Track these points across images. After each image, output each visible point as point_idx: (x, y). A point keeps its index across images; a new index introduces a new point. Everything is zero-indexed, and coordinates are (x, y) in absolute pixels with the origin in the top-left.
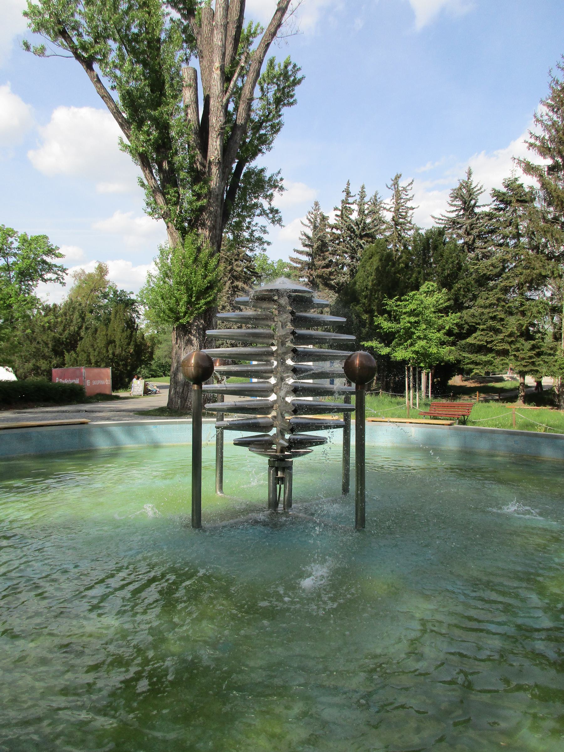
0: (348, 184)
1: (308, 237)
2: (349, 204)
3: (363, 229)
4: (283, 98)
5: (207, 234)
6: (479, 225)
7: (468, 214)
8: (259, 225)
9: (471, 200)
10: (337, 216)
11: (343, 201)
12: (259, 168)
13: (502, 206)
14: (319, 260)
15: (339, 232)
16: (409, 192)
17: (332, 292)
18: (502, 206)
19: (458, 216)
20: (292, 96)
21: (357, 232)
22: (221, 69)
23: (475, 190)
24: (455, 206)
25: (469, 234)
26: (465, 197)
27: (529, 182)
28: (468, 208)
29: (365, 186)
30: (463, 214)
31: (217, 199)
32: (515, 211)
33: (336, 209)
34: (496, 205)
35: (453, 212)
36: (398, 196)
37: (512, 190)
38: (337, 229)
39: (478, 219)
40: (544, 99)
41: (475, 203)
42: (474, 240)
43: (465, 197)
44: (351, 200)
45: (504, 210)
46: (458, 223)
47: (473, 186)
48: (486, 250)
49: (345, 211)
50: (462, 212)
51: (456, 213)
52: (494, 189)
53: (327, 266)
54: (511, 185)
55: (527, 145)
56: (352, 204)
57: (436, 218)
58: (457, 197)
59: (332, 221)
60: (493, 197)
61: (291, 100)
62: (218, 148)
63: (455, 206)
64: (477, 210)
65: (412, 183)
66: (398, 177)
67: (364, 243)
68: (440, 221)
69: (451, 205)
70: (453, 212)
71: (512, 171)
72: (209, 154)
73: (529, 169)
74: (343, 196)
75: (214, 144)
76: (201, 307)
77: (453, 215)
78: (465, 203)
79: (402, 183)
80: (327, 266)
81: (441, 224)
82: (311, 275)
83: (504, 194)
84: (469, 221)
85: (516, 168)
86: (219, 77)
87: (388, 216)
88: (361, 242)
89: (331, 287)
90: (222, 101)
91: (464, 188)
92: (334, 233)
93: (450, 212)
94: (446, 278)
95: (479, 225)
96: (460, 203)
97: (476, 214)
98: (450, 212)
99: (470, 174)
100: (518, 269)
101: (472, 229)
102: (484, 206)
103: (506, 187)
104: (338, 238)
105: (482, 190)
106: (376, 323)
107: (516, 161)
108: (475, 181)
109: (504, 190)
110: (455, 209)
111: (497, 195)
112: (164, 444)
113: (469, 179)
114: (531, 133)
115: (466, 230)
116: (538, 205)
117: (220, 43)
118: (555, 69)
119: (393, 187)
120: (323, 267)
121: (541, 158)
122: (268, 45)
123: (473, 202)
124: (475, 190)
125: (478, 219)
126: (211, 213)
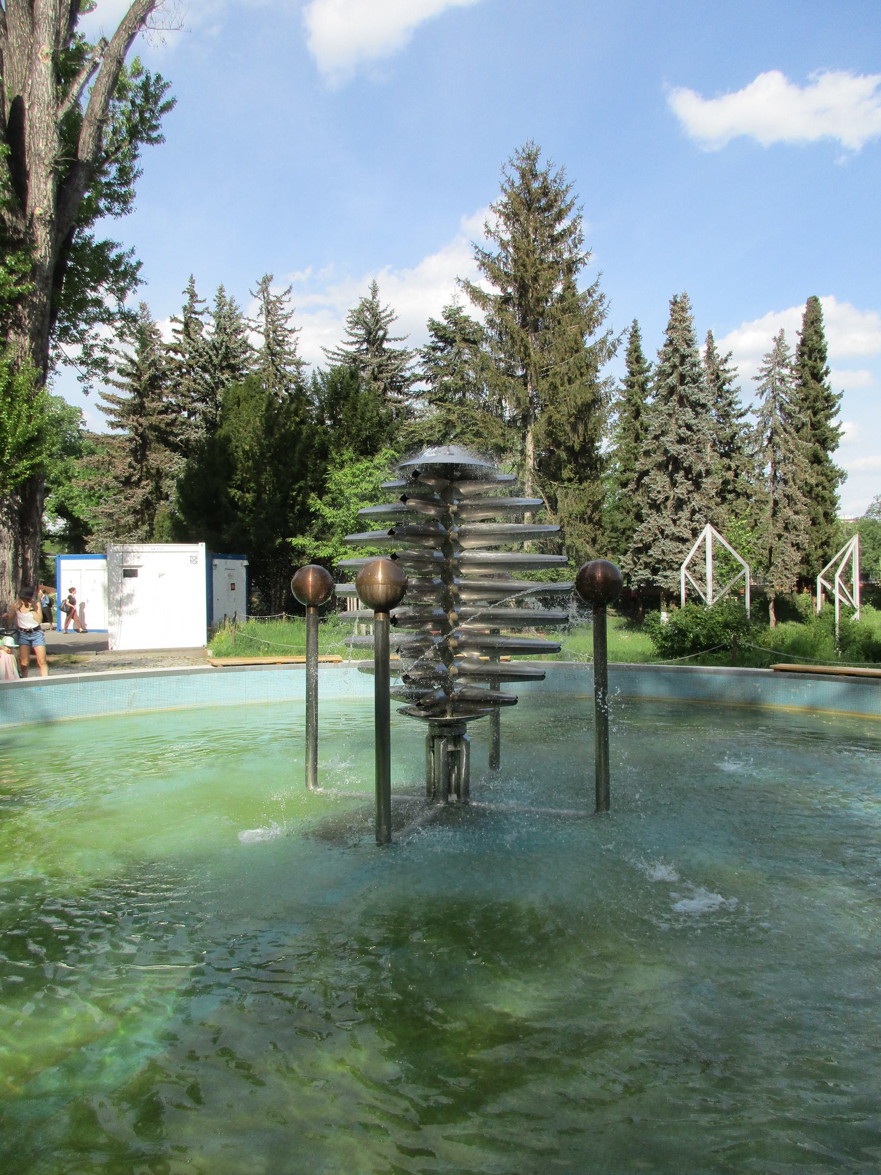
0: (192, 281)
1: (132, 361)
2: (195, 313)
3: (226, 357)
4: (141, 129)
5: (27, 343)
6: (390, 367)
7: (374, 349)
8: (102, 337)
9: (379, 329)
10: (175, 331)
11: (185, 308)
12: (97, 241)
13: (441, 344)
14: (153, 400)
15: (179, 357)
16: (284, 305)
17: (177, 456)
18: (441, 344)
19: (359, 350)
20: (155, 128)
21: (216, 361)
22: (53, 59)
23: (383, 315)
24: (356, 335)
25: (376, 379)
26: (371, 326)
27: (477, 315)
28: (375, 341)
29: (225, 288)
30: (367, 349)
31: (46, 286)
32: (459, 353)
33: (174, 320)
34: (433, 342)
35: (352, 343)
36: (270, 309)
37: (456, 324)
38: (176, 352)
39: (389, 358)
40: (494, 204)
41: (385, 335)
42: (385, 390)
43: (371, 326)
44: (198, 307)
45: (442, 350)
46: (362, 362)
47: (380, 309)
48: (403, 405)
49: (189, 327)
50: (365, 346)
51: (357, 346)
52: (431, 320)
53: (165, 411)
54: (453, 315)
55: (478, 263)
56: (201, 313)
57: (329, 352)
58: (357, 323)
59: (168, 338)
60: (430, 330)
61: (154, 135)
62: (50, 195)
63: (356, 335)
64: (386, 345)
65: (289, 291)
66: (267, 280)
67: (227, 379)
68: (336, 356)
69: (351, 334)
70: (352, 343)
71: (454, 297)
72: (31, 202)
73: (477, 296)
74: (186, 300)
75: (42, 186)
76: (22, 473)
77: (352, 349)
78: (369, 333)
79: (275, 290)
80: (165, 411)
81: (335, 360)
82: (141, 425)
83: (445, 328)
84: (376, 361)
85: (461, 294)
86: (50, 72)
87: (257, 341)
88: (223, 378)
89: (174, 448)
90: (55, 114)
91: (368, 310)
92: (172, 359)
93: (347, 343)
94: (364, 442)
95: (390, 367)
96: (362, 332)
97: (384, 351)
98: (347, 343)
99: (375, 291)
100: (467, 436)
101: (381, 372)
102: (396, 340)
103: (446, 318)
104: (179, 368)
105: (394, 317)
106: (312, 510)
107: (462, 284)
108: (384, 302)
109: (444, 322)
110: (355, 340)
111: (435, 328)
112: (58, 719)
113: (374, 297)
114: (476, 247)
115: (373, 373)
116: (485, 347)
117: (51, 13)
118: (508, 166)
119: (261, 295)
120: (161, 413)
121: (489, 284)
122: (131, 37)
123: (381, 333)
124: (383, 315)
125: (389, 358)
126: (33, 306)
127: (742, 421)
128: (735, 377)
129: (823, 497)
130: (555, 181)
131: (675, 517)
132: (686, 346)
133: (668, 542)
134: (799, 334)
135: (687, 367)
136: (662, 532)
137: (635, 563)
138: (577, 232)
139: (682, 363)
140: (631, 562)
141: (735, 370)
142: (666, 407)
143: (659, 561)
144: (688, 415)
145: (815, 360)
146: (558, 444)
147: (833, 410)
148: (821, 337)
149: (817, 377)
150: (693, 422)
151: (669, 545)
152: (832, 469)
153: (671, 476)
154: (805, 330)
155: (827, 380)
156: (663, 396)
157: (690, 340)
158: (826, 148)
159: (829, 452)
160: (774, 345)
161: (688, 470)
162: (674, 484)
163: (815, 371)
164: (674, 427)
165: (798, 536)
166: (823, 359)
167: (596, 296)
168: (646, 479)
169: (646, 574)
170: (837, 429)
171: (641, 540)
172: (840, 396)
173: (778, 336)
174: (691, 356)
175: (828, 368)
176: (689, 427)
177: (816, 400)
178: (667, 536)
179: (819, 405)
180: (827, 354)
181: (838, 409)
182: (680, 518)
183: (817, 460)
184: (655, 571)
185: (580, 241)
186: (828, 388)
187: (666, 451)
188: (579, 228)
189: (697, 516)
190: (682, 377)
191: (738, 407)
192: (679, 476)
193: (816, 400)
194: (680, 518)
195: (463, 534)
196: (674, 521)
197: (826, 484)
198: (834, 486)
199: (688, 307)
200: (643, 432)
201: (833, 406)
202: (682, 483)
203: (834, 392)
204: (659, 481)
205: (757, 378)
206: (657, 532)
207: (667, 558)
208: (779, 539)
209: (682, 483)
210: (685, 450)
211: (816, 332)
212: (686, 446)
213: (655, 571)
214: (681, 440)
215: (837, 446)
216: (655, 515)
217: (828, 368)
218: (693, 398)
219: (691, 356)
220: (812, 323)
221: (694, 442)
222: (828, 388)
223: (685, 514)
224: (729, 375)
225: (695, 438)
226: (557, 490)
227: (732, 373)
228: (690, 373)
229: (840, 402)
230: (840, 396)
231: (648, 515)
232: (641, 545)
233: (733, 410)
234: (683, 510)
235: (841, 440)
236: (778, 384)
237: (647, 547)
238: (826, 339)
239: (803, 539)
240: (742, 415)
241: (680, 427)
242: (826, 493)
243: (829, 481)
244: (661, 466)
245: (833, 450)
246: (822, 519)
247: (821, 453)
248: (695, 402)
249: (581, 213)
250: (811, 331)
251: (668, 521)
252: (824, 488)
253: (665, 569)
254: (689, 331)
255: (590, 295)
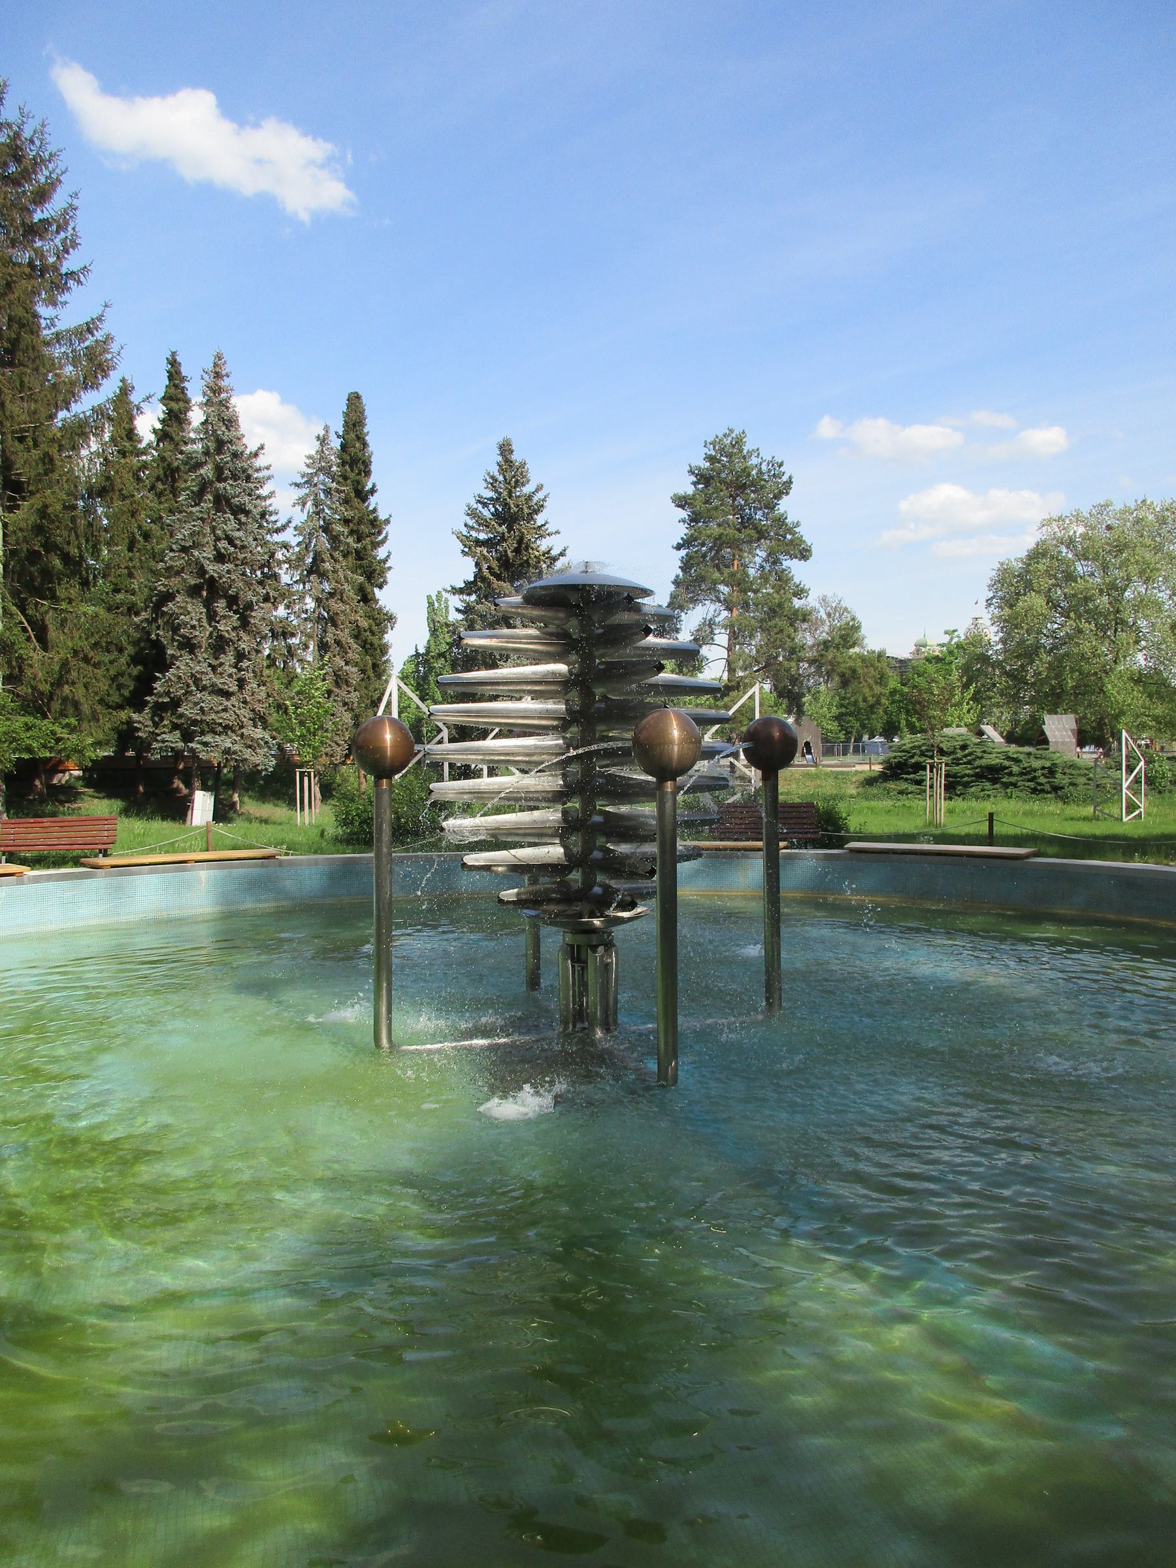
127: (277, 538)
128: (269, 478)
129: (372, 644)
130: (32, 142)
131: (215, 663)
132: (224, 428)
133: (206, 696)
134: (339, 437)
135: (226, 457)
136: (197, 681)
137: (156, 725)
138: (70, 228)
139: (219, 451)
140: (150, 723)
141: (268, 468)
142: (198, 508)
143: (195, 722)
144: (229, 525)
145: (359, 474)
146: (50, 547)
147: (380, 538)
148: (365, 445)
149: (362, 495)
150: (237, 534)
151: (210, 700)
152: (380, 610)
153: (208, 604)
154: (346, 432)
155: (373, 501)
156: (192, 492)
157: (229, 421)
158: (265, 208)
159: (376, 590)
160: (317, 445)
161: (232, 601)
162: (212, 616)
163: (360, 487)
164: (210, 539)
165: (349, 692)
166: (368, 473)
167: (99, 335)
168: (170, 607)
169: (173, 739)
170: (385, 561)
171: (168, 693)
172: (387, 521)
173: (322, 433)
174: (231, 442)
175: (374, 486)
176: (231, 541)
177: (360, 522)
178: (204, 688)
179: (364, 529)
180: (373, 468)
181: (386, 537)
182: (221, 664)
183: (366, 598)
184: (187, 737)
185: (74, 245)
186: (375, 510)
187: (202, 571)
188: (72, 224)
189: (245, 664)
190: (219, 470)
191: (273, 518)
192: (220, 605)
193: (360, 522)
194: (221, 664)
195: (558, 797)
196: (214, 668)
197: (375, 628)
198: (384, 632)
199: (224, 373)
200: (141, 539)
201: (380, 533)
202: (224, 617)
203: (382, 516)
204: (191, 612)
205: (297, 485)
206: (190, 682)
207: (208, 718)
208: (329, 697)
209: (224, 617)
210: (229, 572)
211: (358, 438)
212: (231, 566)
213: (187, 737)
214: (220, 558)
215: (385, 582)
216: (187, 657)
217: (374, 486)
218: (236, 501)
219: (231, 442)
220: (354, 425)
221: (239, 562)
222: (375, 510)
223: (228, 658)
224: (260, 475)
225: (241, 556)
226: (47, 612)
227: (265, 473)
228: (230, 465)
229: (388, 528)
230: (387, 521)
231: (176, 658)
232: (167, 700)
233: (267, 521)
234: (224, 653)
235: (389, 576)
236: (322, 496)
237: (175, 703)
238: (370, 449)
239: (354, 697)
240: (278, 531)
241: (218, 539)
242: (375, 640)
243: (377, 625)
244: (194, 591)
245: (381, 587)
246: (370, 673)
247: (367, 586)
248: (237, 506)
249: (75, 202)
250: (353, 435)
251: (204, 667)
252: (373, 634)
253: (203, 733)
254: (228, 408)
255: (89, 331)
